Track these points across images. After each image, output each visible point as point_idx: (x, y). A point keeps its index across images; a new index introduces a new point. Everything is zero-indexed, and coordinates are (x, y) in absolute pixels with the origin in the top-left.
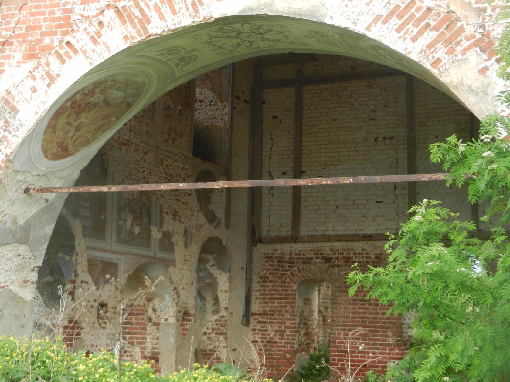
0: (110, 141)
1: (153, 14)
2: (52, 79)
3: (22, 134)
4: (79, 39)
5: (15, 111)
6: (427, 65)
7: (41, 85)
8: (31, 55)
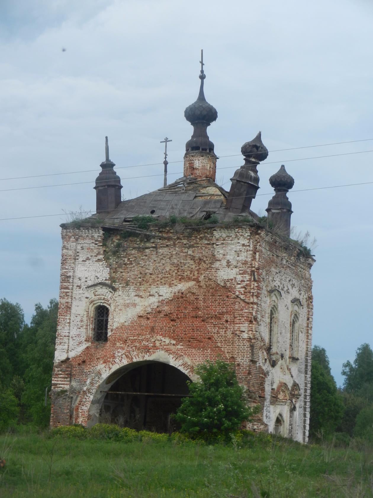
0: (105, 318)
1: (134, 357)
2: (110, 369)
3: (103, 380)
4: (117, 360)
5: (101, 375)
6: (188, 375)
7: (108, 369)
8: (105, 362)
